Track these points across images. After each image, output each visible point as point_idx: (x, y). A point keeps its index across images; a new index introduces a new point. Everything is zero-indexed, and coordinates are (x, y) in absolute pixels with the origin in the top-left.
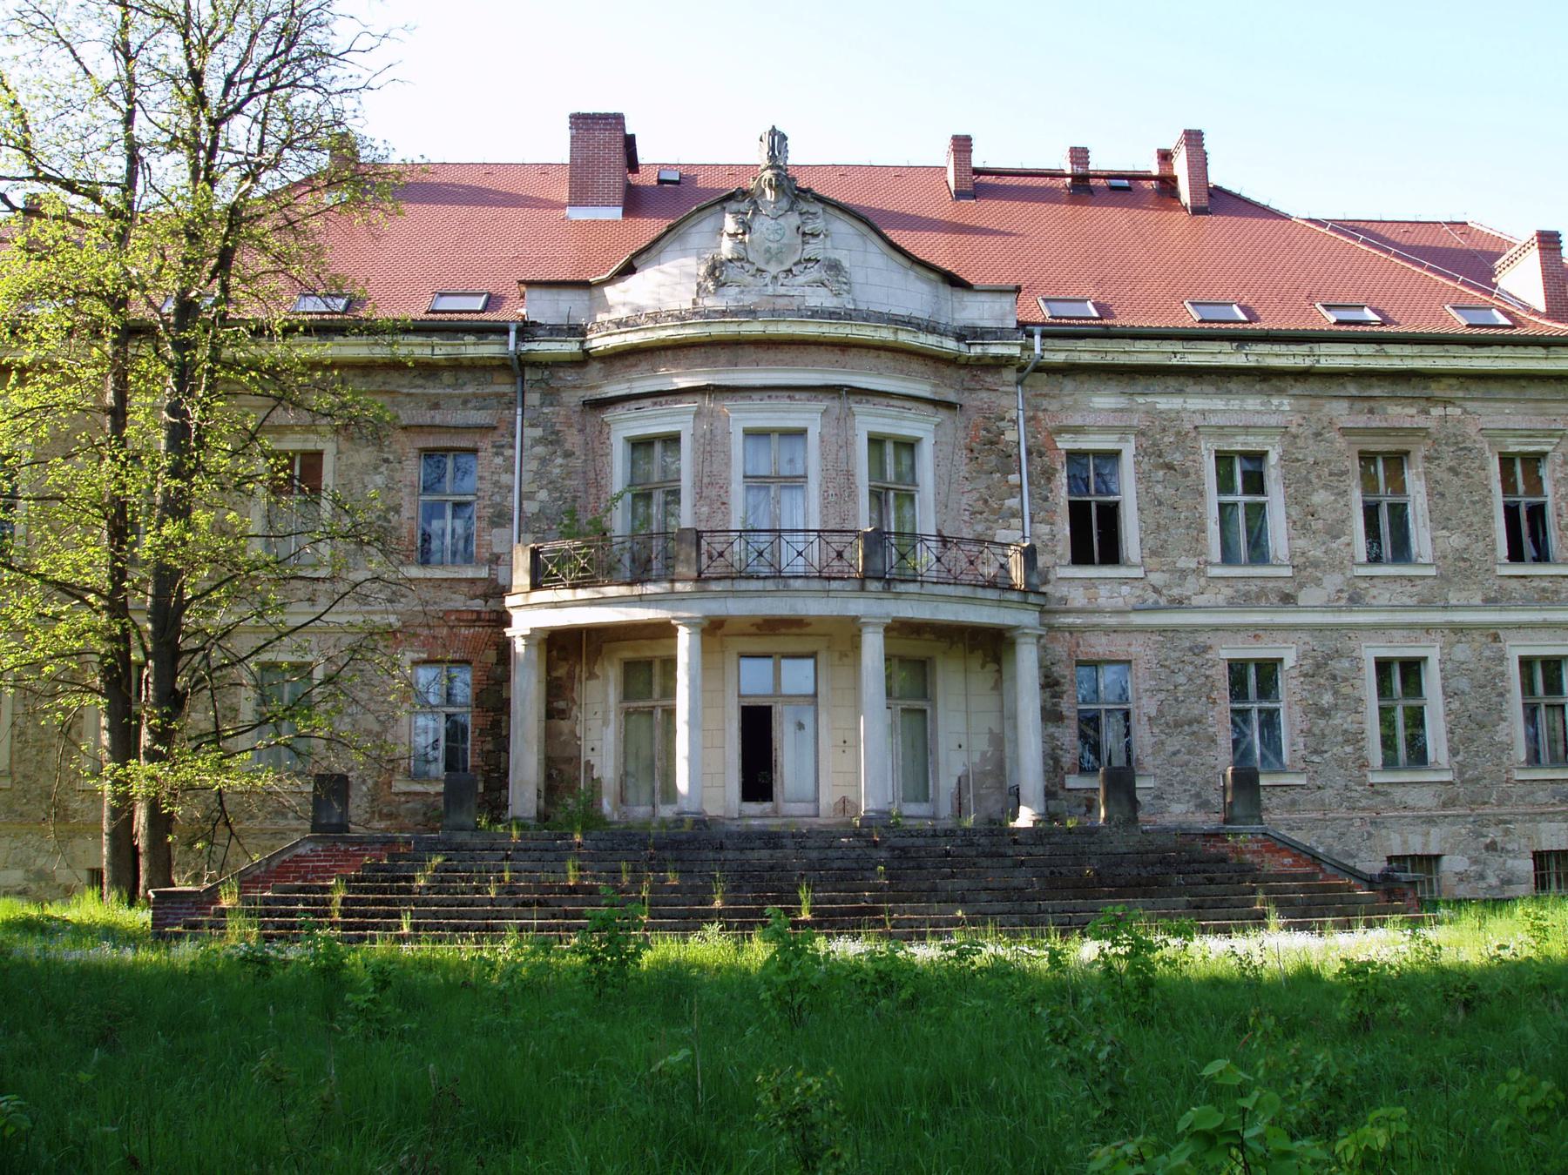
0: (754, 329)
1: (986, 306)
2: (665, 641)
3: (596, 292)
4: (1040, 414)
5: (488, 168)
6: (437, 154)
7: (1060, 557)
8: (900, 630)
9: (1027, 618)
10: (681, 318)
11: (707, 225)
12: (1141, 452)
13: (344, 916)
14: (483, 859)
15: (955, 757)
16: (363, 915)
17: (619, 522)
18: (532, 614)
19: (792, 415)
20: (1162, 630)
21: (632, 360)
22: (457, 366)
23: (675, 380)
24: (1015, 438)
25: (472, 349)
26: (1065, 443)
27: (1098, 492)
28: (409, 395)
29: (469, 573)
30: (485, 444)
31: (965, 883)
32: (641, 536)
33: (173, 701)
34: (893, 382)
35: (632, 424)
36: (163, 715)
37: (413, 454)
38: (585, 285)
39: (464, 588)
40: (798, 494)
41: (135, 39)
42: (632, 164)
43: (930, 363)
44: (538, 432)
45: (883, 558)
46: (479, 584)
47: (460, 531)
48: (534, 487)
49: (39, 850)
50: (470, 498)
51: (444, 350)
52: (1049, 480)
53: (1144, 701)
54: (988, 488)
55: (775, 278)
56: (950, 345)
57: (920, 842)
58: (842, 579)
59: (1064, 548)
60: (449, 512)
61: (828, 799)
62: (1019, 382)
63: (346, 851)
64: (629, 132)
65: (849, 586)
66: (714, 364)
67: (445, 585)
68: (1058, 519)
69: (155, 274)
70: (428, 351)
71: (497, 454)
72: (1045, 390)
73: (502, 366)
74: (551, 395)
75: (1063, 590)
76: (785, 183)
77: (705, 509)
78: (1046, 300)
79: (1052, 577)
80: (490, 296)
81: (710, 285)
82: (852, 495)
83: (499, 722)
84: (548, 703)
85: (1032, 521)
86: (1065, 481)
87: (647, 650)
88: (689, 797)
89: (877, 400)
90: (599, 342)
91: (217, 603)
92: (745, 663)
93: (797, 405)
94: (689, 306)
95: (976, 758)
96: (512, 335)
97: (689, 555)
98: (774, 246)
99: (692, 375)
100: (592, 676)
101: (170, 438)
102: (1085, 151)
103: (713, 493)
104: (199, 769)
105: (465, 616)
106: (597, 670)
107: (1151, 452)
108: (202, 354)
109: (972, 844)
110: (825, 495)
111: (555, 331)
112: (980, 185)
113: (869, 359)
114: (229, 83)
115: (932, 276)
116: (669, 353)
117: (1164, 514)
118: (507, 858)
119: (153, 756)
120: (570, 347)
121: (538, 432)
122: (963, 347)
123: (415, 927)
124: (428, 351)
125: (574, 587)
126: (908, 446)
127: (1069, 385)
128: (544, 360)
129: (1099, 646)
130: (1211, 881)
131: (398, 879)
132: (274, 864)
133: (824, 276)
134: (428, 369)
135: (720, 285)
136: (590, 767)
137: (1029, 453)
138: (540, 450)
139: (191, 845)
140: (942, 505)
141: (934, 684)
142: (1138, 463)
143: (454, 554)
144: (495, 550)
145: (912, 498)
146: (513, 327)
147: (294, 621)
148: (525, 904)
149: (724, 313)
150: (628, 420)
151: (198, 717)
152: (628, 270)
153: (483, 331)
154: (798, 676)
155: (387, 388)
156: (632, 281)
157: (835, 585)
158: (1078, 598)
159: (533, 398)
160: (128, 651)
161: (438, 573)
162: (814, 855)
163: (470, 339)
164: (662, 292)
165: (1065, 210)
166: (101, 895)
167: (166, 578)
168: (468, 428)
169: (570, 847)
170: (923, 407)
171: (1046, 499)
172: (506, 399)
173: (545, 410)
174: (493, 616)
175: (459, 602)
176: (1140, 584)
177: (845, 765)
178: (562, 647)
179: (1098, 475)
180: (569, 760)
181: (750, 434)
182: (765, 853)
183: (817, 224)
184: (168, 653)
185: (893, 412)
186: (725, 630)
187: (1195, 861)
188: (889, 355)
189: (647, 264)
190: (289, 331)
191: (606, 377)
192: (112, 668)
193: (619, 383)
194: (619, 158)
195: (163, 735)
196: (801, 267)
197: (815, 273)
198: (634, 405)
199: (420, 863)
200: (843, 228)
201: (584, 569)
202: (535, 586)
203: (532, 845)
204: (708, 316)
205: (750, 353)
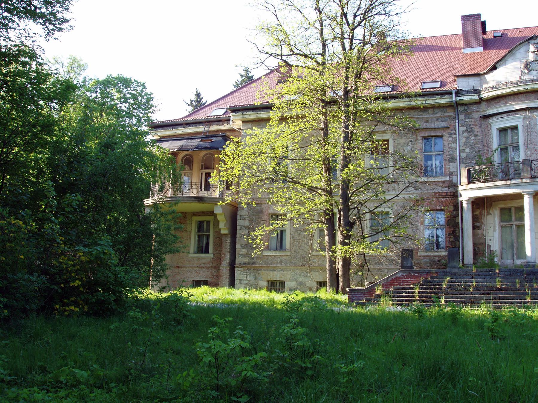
2: (521, 200)
3: (482, 77)
5: (432, 38)
6: (426, 33)
10: (516, 84)
11: (523, 49)
13: (420, 297)
14: (464, 278)
16: (427, 297)
17: (496, 159)
18: (467, 193)
21: (498, 100)
22: (434, 107)
23: (515, 106)
25: (439, 100)
28: (417, 118)
29: (443, 179)
30: (446, 134)
32: (506, 162)
33: (350, 225)
35: (499, 123)
36: (346, 230)
38: (478, 75)
39: (441, 184)
42: (484, 32)
44: (465, 128)
46: (446, 183)
48: (464, 148)
49: (300, 275)
51: (429, 102)
63: (414, 275)
64: (483, 20)
66: (529, 99)
67: (434, 183)
69: (335, 82)
71: (450, 137)
74: (468, 115)
80: (441, 82)
81: (526, 71)
83: (455, 231)
84: (473, 224)
87: (514, 204)
88: (531, 257)
90: (485, 95)
91: (362, 192)
94: (518, 79)
96: (454, 94)
97: (527, 169)
99: (521, 104)
100: (489, 214)
103: (532, 146)
104: (359, 249)
106: (491, 212)
108: (351, 108)
111: (469, 92)
114: (355, 16)
116: (512, 97)
118: (473, 278)
120: (475, 97)
121: (465, 128)
125: (484, 182)
128: (465, 102)
131: (435, 285)
132: (389, 279)
134: (425, 109)
135: (530, 71)
136: (489, 246)
138: (465, 134)
139: (356, 273)
144: (451, 171)
146: (454, 92)
147: (388, 197)
148: (484, 294)
149: (532, 81)
150: (498, 122)
152: (494, 68)
153: (442, 94)
156: (495, 72)
159: (462, 116)
161: (431, 179)
164: (508, 75)
166: (326, 290)
167: (346, 185)
168: (439, 128)
169: (495, 274)
172: (452, 118)
173: (467, 120)
174: (452, 194)
175: (439, 189)
178: (479, 204)
180: (481, 244)
184: (346, 209)
189: (501, 65)
190: (377, 99)
193: (493, 109)
195: (347, 237)
198: (500, 116)
199: (443, 280)
201: (487, 176)
202: (469, 182)
203: (481, 273)
204: (526, 82)
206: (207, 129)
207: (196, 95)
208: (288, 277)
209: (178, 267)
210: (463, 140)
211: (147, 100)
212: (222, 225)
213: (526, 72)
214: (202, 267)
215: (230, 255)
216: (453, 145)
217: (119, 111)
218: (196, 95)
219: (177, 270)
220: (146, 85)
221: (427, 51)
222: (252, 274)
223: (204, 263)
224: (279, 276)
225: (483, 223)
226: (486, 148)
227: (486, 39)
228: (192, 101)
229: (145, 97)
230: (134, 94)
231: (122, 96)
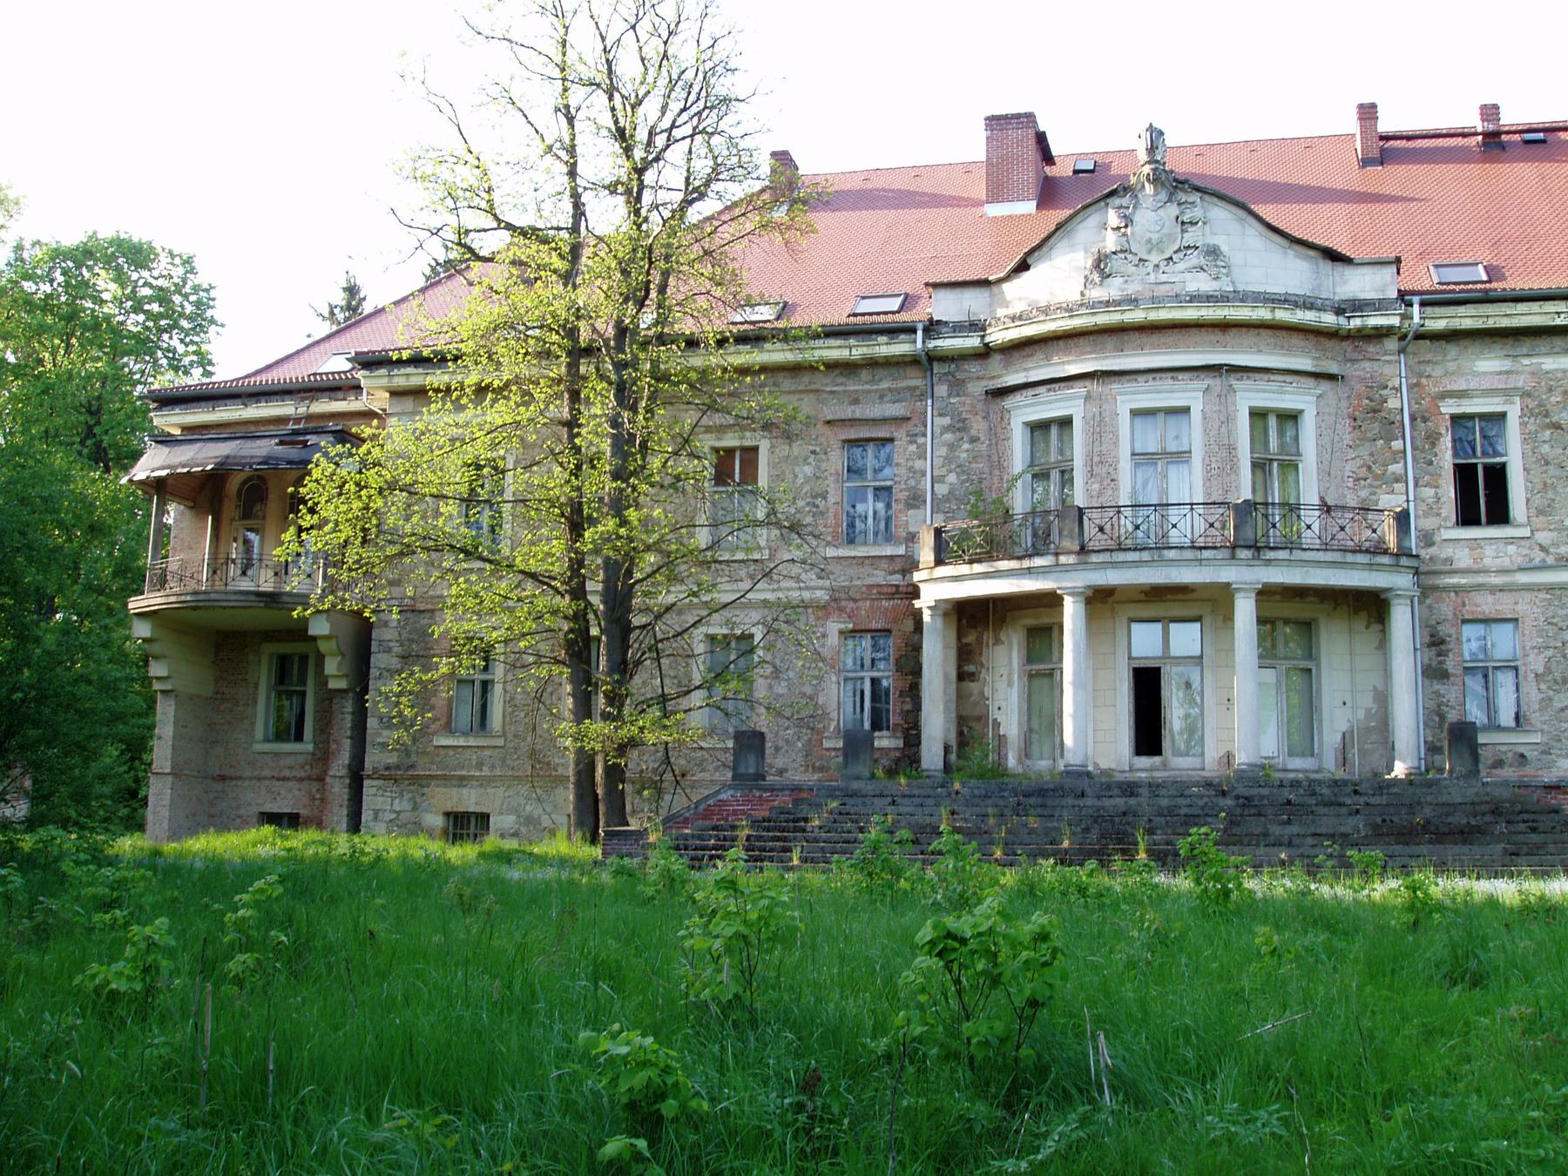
0: (1136, 316)
1: (1367, 278)
3: (995, 289)
4: (1424, 381)
5: (917, 172)
7: (1445, 519)
8: (1266, 594)
9: (1401, 581)
10: (1070, 310)
11: (1093, 220)
12: (1526, 412)
15: (1338, 716)
17: (1019, 502)
18: (939, 586)
19: (1175, 395)
20: (1549, 588)
21: (1028, 350)
22: (873, 363)
24: (1398, 405)
25: (886, 348)
26: (1449, 408)
27: (1484, 454)
28: (832, 392)
29: (889, 551)
30: (900, 434)
31: (1294, 829)
34: (1273, 358)
37: (836, 445)
38: (984, 283)
40: (1184, 468)
41: (573, 103)
42: (1047, 158)
43: (1311, 337)
44: (947, 421)
45: (1250, 528)
47: (882, 513)
48: (944, 471)
49: (528, 798)
50: (888, 483)
52: (1433, 445)
53: (1531, 658)
54: (1372, 454)
55: (1157, 266)
56: (1329, 319)
57: (1265, 791)
58: (1215, 548)
59: (1449, 508)
60: (870, 497)
61: (1212, 753)
62: (1402, 351)
65: (1220, 554)
66: (1102, 350)
68: (1442, 482)
69: (597, 301)
70: (846, 353)
72: (1428, 357)
73: (913, 361)
74: (957, 386)
75: (1448, 552)
76: (1163, 177)
77: (1096, 486)
78: (1436, 266)
79: (1437, 538)
80: (907, 296)
81: (1096, 277)
82: (1234, 468)
84: (959, 667)
85: (1416, 485)
86: (1449, 445)
89: (1257, 376)
90: (997, 336)
92: (1134, 626)
93: (1179, 385)
94: (1078, 297)
95: (1361, 714)
96: (920, 333)
97: (1072, 530)
98: (1155, 237)
99: (1081, 361)
100: (997, 641)
101: (613, 446)
102: (1496, 107)
105: (885, 590)
106: (1003, 637)
107: (1538, 412)
109: (1314, 794)
110: (1208, 468)
111: (959, 328)
112: (1388, 150)
113: (1249, 337)
115: (1312, 253)
116: (1061, 343)
117: (1551, 473)
119: (606, 717)
120: (973, 342)
121: (947, 421)
122: (1342, 321)
123: (804, 860)
124: (846, 353)
125: (971, 562)
126: (1290, 418)
127: (1452, 350)
128: (950, 354)
129: (1486, 604)
130: (1534, 830)
131: (798, 820)
132: (701, 808)
133: (1203, 261)
135: (1105, 276)
136: (997, 724)
137: (1413, 419)
138: (948, 437)
140: (1325, 473)
141: (1318, 647)
142: (1523, 424)
143: (876, 534)
144: (911, 529)
145: (1296, 467)
146: (920, 326)
150: (1025, 406)
151: (644, 683)
152: (1023, 267)
153: (893, 331)
154: (1186, 638)
155: (813, 387)
156: (1026, 276)
157: (1206, 554)
158: (1463, 559)
159: (942, 390)
160: (588, 630)
161: (861, 551)
162: (1164, 802)
163: (883, 339)
165: (1474, 169)
168: (885, 420)
170: (1303, 380)
171: (1430, 463)
172: (918, 392)
175: (880, 577)
176: (1526, 543)
177: (1235, 719)
178: (971, 616)
179: (1484, 437)
180: (979, 718)
181: (1135, 413)
182: (1120, 801)
183: (1197, 213)
185: (1273, 386)
186: (1117, 596)
187: (1527, 812)
188: (1270, 332)
191: (1006, 367)
192: (575, 642)
194: (1031, 152)
196: (1181, 255)
197: (1194, 259)
198: (1030, 392)
200: (1220, 214)
201: (980, 546)
202: (939, 562)
203: (916, 792)
204: (1094, 306)
205: (1135, 336)
206: (302, 410)
207: (345, 289)
208: (498, 803)
209: (223, 778)
210: (943, 451)
211: (198, 304)
212: (331, 666)
213: (1097, 280)
214: (284, 779)
215: (353, 746)
216: (918, 464)
217: (117, 331)
218: (345, 289)
219: (219, 786)
220: (197, 263)
221: (896, 207)
222: (407, 796)
223: (291, 768)
224: (473, 800)
225: (982, 665)
226: (997, 472)
227: (1054, 178)
228: (332, 308)
229: (193, 298)
230: (161, 289)
231: (129, 290)
